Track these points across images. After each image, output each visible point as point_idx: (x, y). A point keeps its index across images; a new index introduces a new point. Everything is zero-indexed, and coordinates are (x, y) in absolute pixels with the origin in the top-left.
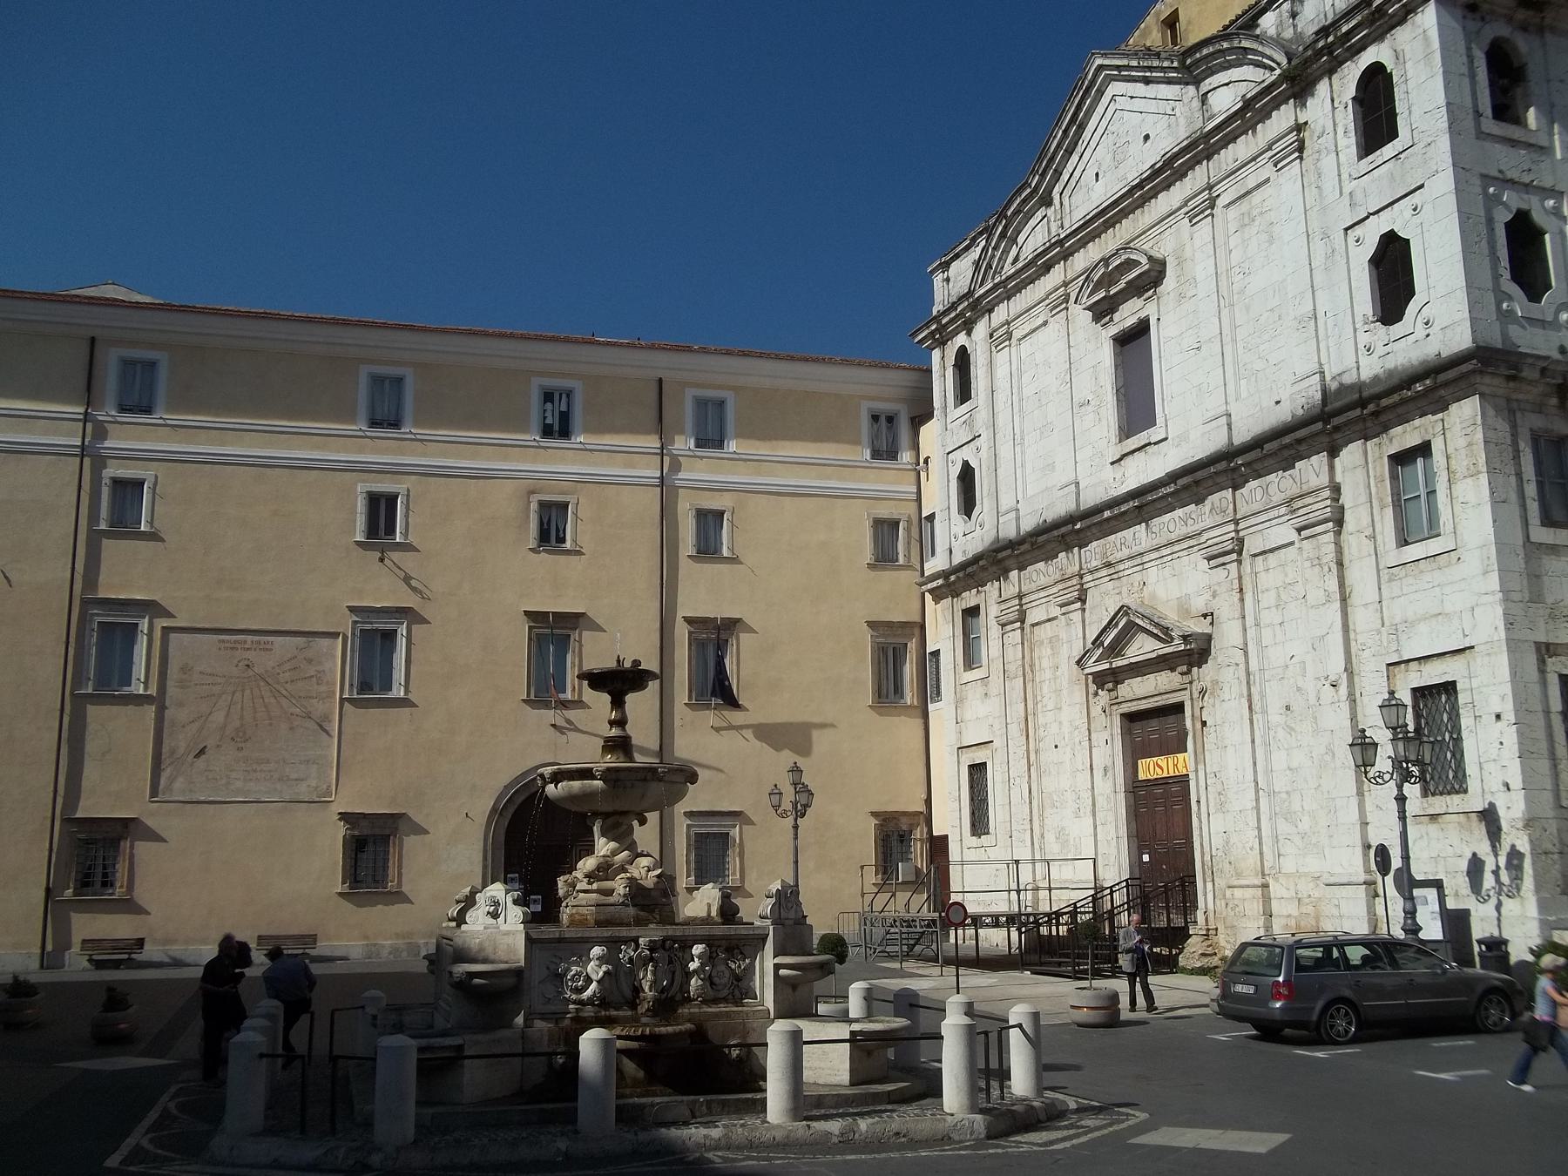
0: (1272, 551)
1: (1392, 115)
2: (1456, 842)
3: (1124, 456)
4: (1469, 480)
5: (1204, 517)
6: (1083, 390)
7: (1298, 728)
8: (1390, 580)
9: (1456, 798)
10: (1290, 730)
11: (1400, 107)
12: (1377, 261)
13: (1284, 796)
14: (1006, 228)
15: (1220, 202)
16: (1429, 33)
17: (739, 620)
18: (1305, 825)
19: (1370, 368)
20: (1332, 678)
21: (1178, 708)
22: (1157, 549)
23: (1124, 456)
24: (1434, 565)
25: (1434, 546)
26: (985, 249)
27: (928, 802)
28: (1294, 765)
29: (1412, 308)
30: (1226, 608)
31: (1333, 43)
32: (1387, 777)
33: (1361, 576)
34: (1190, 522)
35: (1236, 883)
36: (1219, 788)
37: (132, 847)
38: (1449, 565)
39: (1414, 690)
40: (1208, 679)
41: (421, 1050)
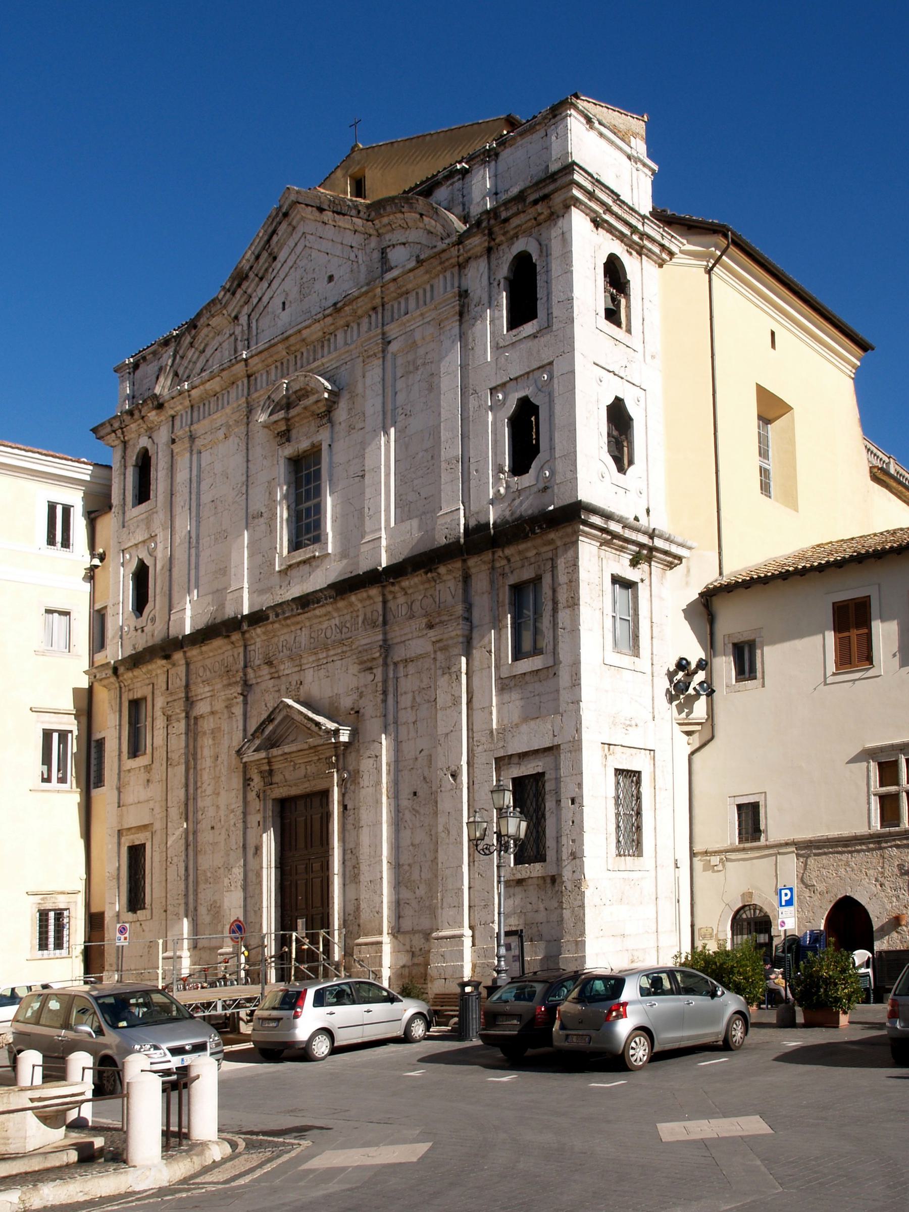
2: (534, 899)
7: (422, 811)
10: (415, 812)
28: (417, 842)
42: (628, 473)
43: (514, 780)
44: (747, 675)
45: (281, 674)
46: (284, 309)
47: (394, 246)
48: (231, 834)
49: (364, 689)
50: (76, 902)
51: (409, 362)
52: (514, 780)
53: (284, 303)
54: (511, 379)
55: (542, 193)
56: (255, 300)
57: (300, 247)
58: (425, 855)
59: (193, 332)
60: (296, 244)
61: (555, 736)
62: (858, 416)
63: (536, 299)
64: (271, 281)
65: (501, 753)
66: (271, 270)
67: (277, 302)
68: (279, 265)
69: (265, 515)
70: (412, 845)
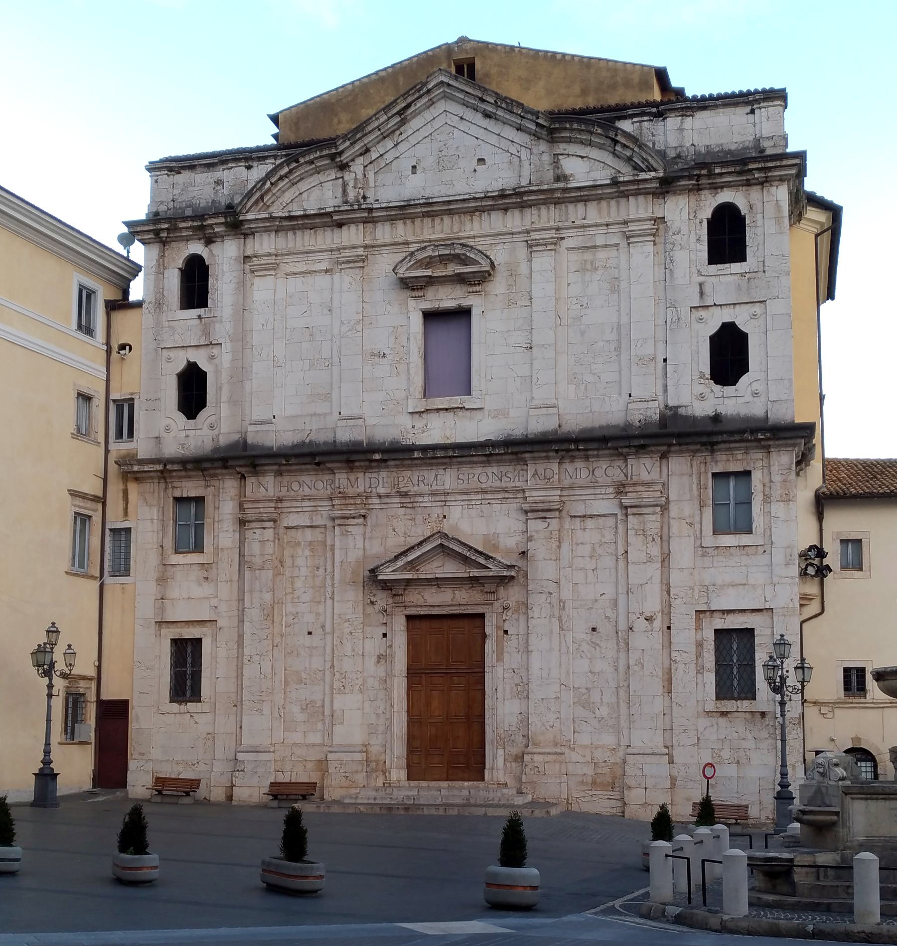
0: (591, 517)
3: (427, 411)
4: (781, 504)
7: (603, 644)
9: (746, 703)
10: (595, 645)
12: (202, 404)
13: (584, 691)
14: (291, 172)
15: (566, 244)
16: (781, 203)
18: (604, 711)
19: (702, 409)
21: (482, 616)
22: (466, 493)
23: (427, 411)
24: (742, 552)
26: (269, 175)
27: (99, 668)
28: (597, 669)
31: (703, 175)
34: (505, 479)
38: (756, 553)
41: (749, 858)
42: (146, 179)
46: (414, 173)
49: (533, 534)
50: (90, 688)
54: (715, 305)
56: (374, 155)
57: (437, 124)
61: (766, 601)
63: (745, 246)
64: (398, 144)
66: (398, 132)
67: (406, 164)
69: (389, 357)
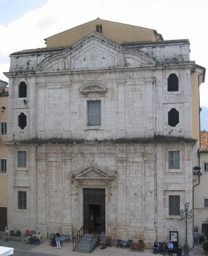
1: (24, 128)
2: (176, 223)
5: (119, 151)
6: (75, 108)
8: (166, 175)
11: (179, 85)
13: (133, 211)
17: (91, 252)
18: (138, 217)
20: (151, 191)
25: (178, 171)
29: (178, 125)
30: (120, 171)
32: (188, 218)
33: (160, 173)
35: (119, 228)
36: (114, 208)
37: (69, 162)
38: (180, 175)
39: (169, 196)
40: (113, 185)
43: (170, 196)
44: (23, 206)
45: (86, 157)
47: (128, 58)
48: (66, 195)
51: (133, 88)
52: (170, 196)
53: (84, 59)
55: (184, 64)
58: (139, 209)
59: (50, 58)
60: (90, 45)
62: (199, 65)
65: (166, 189)
66: (80, 49)
67: (82, 58)
68: (83, 49)
70: (135, 206)
